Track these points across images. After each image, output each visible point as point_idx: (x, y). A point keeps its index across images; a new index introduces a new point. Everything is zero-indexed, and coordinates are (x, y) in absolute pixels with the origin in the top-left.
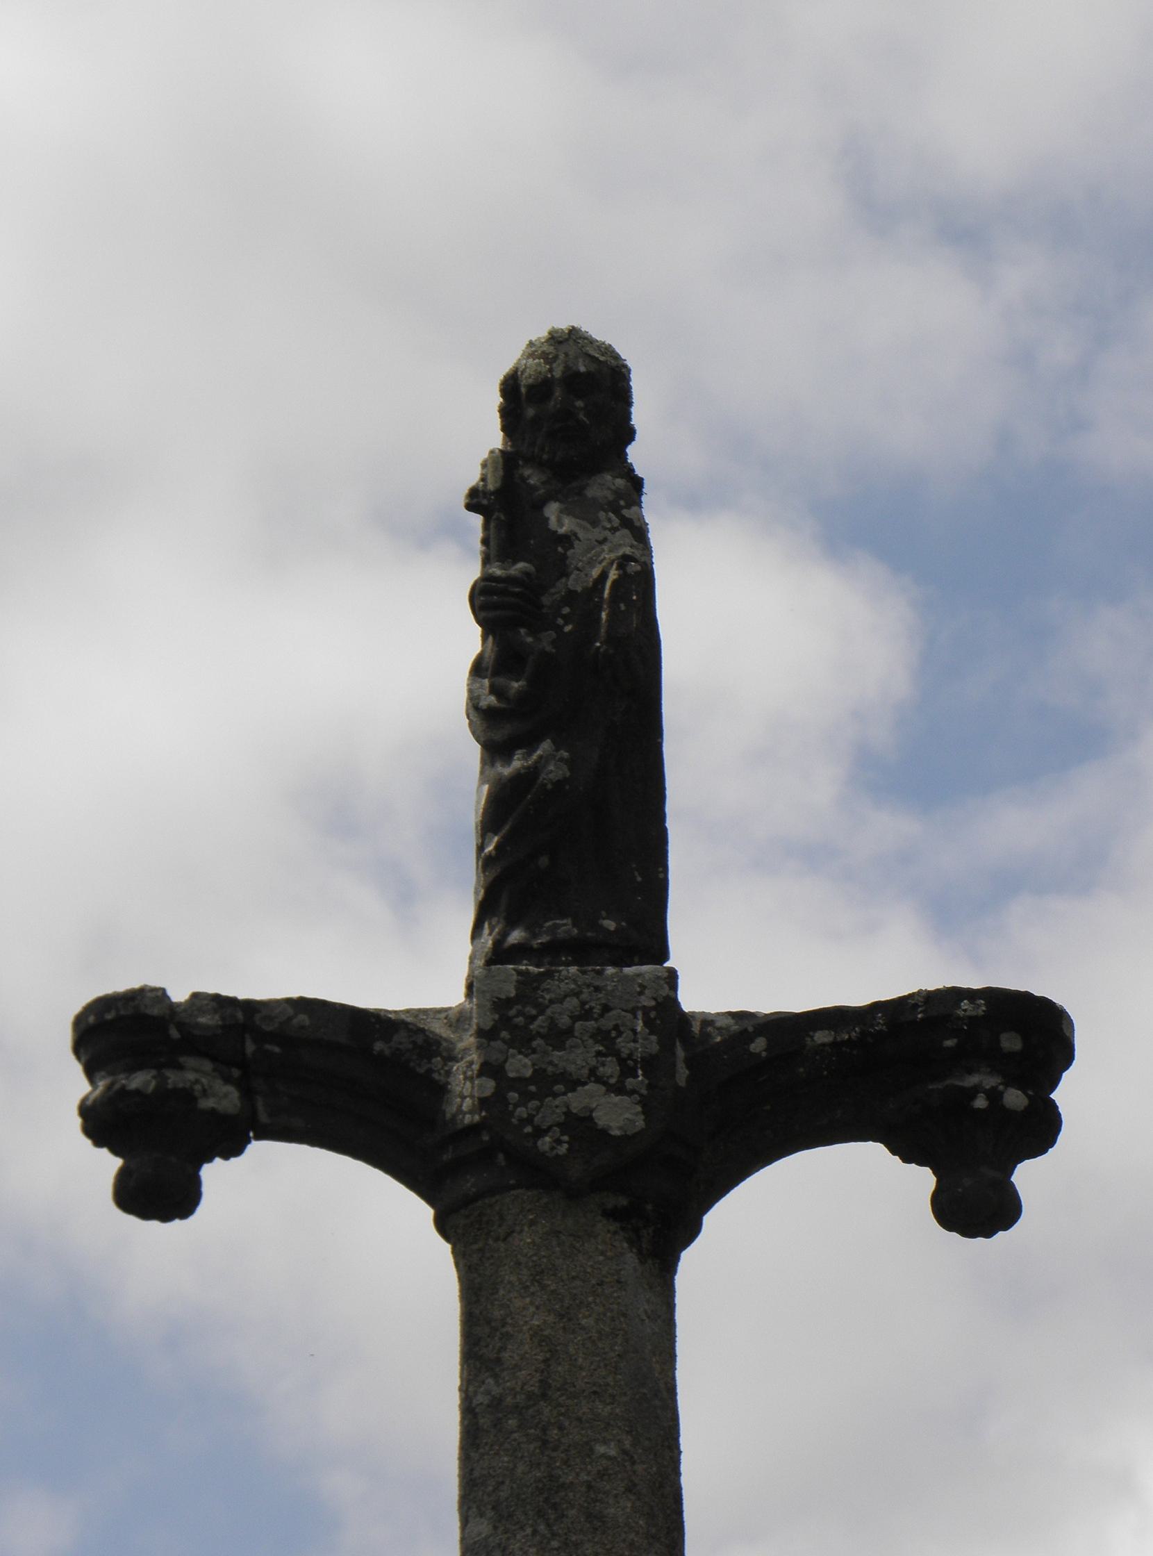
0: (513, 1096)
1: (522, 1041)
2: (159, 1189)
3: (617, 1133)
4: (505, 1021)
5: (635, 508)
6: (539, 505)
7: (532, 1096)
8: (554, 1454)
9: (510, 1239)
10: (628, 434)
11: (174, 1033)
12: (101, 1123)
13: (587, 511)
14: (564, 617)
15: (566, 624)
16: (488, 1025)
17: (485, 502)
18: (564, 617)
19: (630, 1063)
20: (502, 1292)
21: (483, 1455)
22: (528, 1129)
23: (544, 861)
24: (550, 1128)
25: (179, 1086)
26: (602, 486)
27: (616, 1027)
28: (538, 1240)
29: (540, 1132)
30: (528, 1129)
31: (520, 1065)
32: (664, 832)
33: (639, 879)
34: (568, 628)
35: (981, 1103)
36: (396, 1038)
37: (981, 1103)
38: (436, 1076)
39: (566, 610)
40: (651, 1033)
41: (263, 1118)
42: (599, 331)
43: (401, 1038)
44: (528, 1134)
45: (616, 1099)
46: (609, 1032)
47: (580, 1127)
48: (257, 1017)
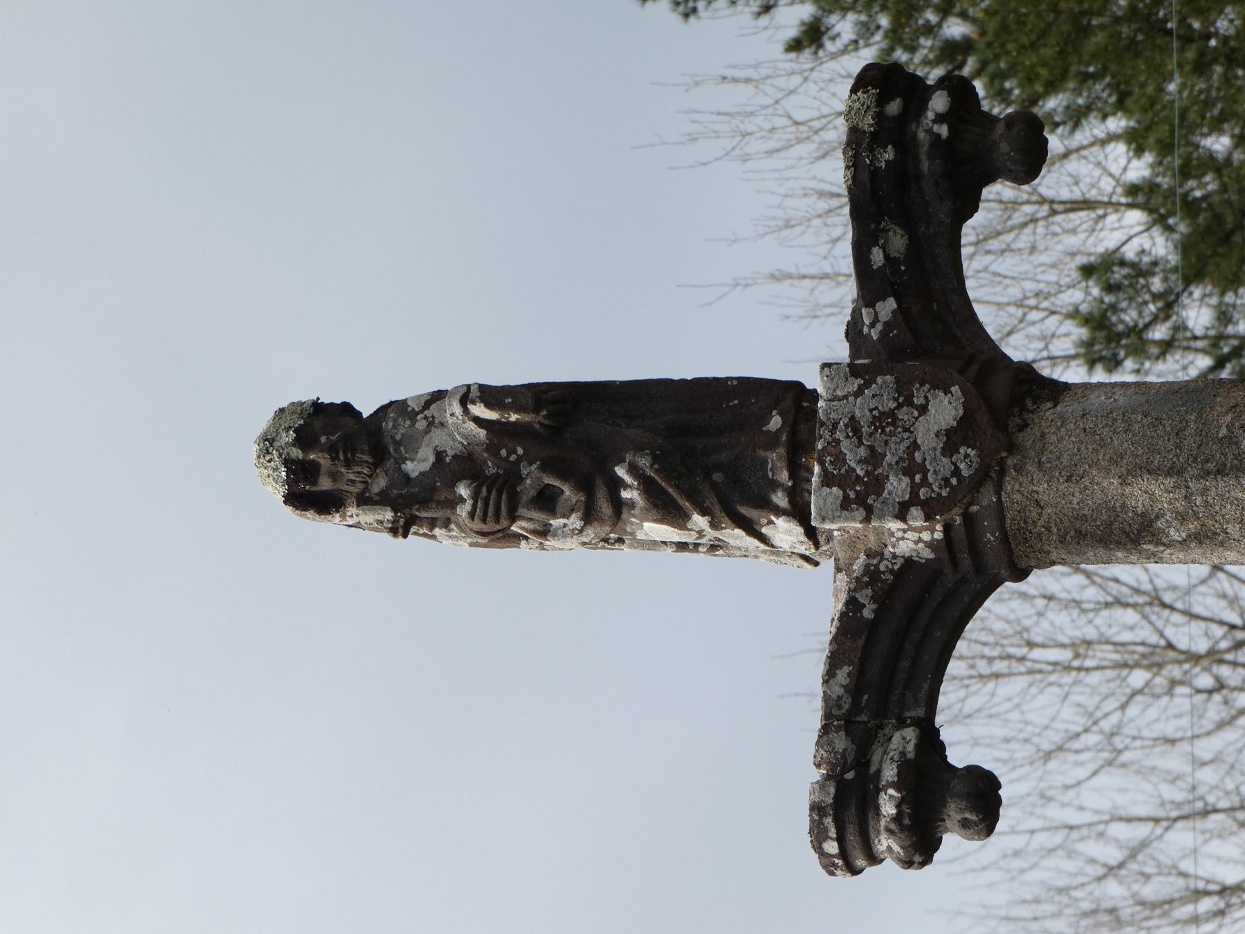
0: (923, 493)
1: (877, 484)
2: (982, 798)
3: (961, 412)
4: (861, 501)
5: (409, 403)
6: (407, 478)
7: (925, 478)
8: (1229, 465)
9: (1042, 503)
10: (346, 408)
11: (850, 775)
12: (921, 847)
13: (411, 444)
14: (509, 454)
15: (515, 452)
16: (862, 513)
17: (402, 522)
18: (509, 454)
19: (901, 400)
20: (1086, 512)
21: (1173, 683)
22: (954, 481)
23: (717, 477)
24: (955, 464)
25: (891, 777)
26: (395, 428)
27: (871, 411)
28: (1047, 478)
29: (956, 472)
30: (954, 481)
31: (898, 486)
32: (697, 381)
33: (736, 402)
34: (520, 451)
35: (943, 130)
36: (861, 600)
37: (943, 130)
38: (896, 567)
39: (504, 452)
40: (875, 382)
41: (920, 712)
42: (262, 421)
43: (864, 597)
44: (958, 481)
45: (932, 410)
46: (874, 417)
47: (952, 439)
48: (835, 712)
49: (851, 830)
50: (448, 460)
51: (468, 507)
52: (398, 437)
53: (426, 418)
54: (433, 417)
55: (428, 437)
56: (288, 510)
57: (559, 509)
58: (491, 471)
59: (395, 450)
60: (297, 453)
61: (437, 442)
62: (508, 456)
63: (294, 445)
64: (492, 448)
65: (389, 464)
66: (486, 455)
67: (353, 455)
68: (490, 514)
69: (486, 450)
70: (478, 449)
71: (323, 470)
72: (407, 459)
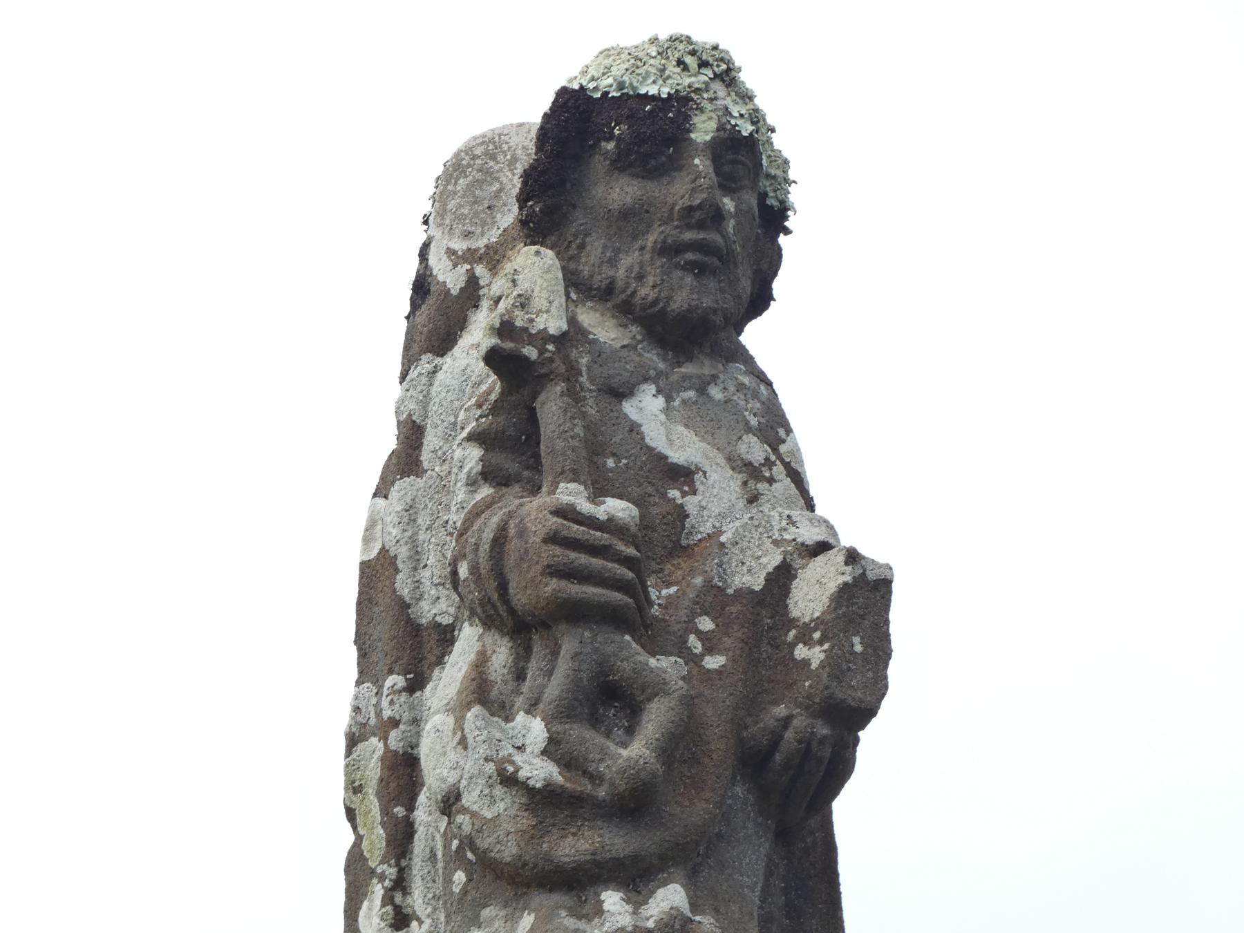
10: (760, 301)
14: (702, 636)
15: (710, 650)
18: (703, 636)
34: (714, 662)
49: (619, 841)
50: (674, 494)
51: (585, 506)
52: (715, 392)
53: (768, 463)
54: (771, 481)
55: (722, 461)
56: (558, 87)
57: (578, 733)
58: (659, 594)
59: (685, 378)
60: (703, 130)
61: (714, 476)
62: (699, 633)
63: (721, 128)
64: (715, 598)
65: (653, 358)
66: (698, 581)
67: (690, 267)
68: (573, 555)
69: (708, 584)
70: (711, 565)
71: (654, 189)
72: (669, 399)
